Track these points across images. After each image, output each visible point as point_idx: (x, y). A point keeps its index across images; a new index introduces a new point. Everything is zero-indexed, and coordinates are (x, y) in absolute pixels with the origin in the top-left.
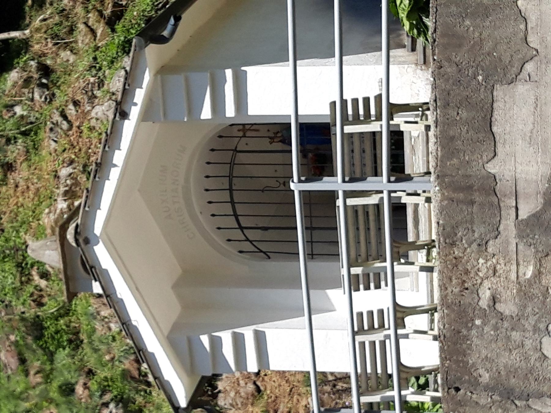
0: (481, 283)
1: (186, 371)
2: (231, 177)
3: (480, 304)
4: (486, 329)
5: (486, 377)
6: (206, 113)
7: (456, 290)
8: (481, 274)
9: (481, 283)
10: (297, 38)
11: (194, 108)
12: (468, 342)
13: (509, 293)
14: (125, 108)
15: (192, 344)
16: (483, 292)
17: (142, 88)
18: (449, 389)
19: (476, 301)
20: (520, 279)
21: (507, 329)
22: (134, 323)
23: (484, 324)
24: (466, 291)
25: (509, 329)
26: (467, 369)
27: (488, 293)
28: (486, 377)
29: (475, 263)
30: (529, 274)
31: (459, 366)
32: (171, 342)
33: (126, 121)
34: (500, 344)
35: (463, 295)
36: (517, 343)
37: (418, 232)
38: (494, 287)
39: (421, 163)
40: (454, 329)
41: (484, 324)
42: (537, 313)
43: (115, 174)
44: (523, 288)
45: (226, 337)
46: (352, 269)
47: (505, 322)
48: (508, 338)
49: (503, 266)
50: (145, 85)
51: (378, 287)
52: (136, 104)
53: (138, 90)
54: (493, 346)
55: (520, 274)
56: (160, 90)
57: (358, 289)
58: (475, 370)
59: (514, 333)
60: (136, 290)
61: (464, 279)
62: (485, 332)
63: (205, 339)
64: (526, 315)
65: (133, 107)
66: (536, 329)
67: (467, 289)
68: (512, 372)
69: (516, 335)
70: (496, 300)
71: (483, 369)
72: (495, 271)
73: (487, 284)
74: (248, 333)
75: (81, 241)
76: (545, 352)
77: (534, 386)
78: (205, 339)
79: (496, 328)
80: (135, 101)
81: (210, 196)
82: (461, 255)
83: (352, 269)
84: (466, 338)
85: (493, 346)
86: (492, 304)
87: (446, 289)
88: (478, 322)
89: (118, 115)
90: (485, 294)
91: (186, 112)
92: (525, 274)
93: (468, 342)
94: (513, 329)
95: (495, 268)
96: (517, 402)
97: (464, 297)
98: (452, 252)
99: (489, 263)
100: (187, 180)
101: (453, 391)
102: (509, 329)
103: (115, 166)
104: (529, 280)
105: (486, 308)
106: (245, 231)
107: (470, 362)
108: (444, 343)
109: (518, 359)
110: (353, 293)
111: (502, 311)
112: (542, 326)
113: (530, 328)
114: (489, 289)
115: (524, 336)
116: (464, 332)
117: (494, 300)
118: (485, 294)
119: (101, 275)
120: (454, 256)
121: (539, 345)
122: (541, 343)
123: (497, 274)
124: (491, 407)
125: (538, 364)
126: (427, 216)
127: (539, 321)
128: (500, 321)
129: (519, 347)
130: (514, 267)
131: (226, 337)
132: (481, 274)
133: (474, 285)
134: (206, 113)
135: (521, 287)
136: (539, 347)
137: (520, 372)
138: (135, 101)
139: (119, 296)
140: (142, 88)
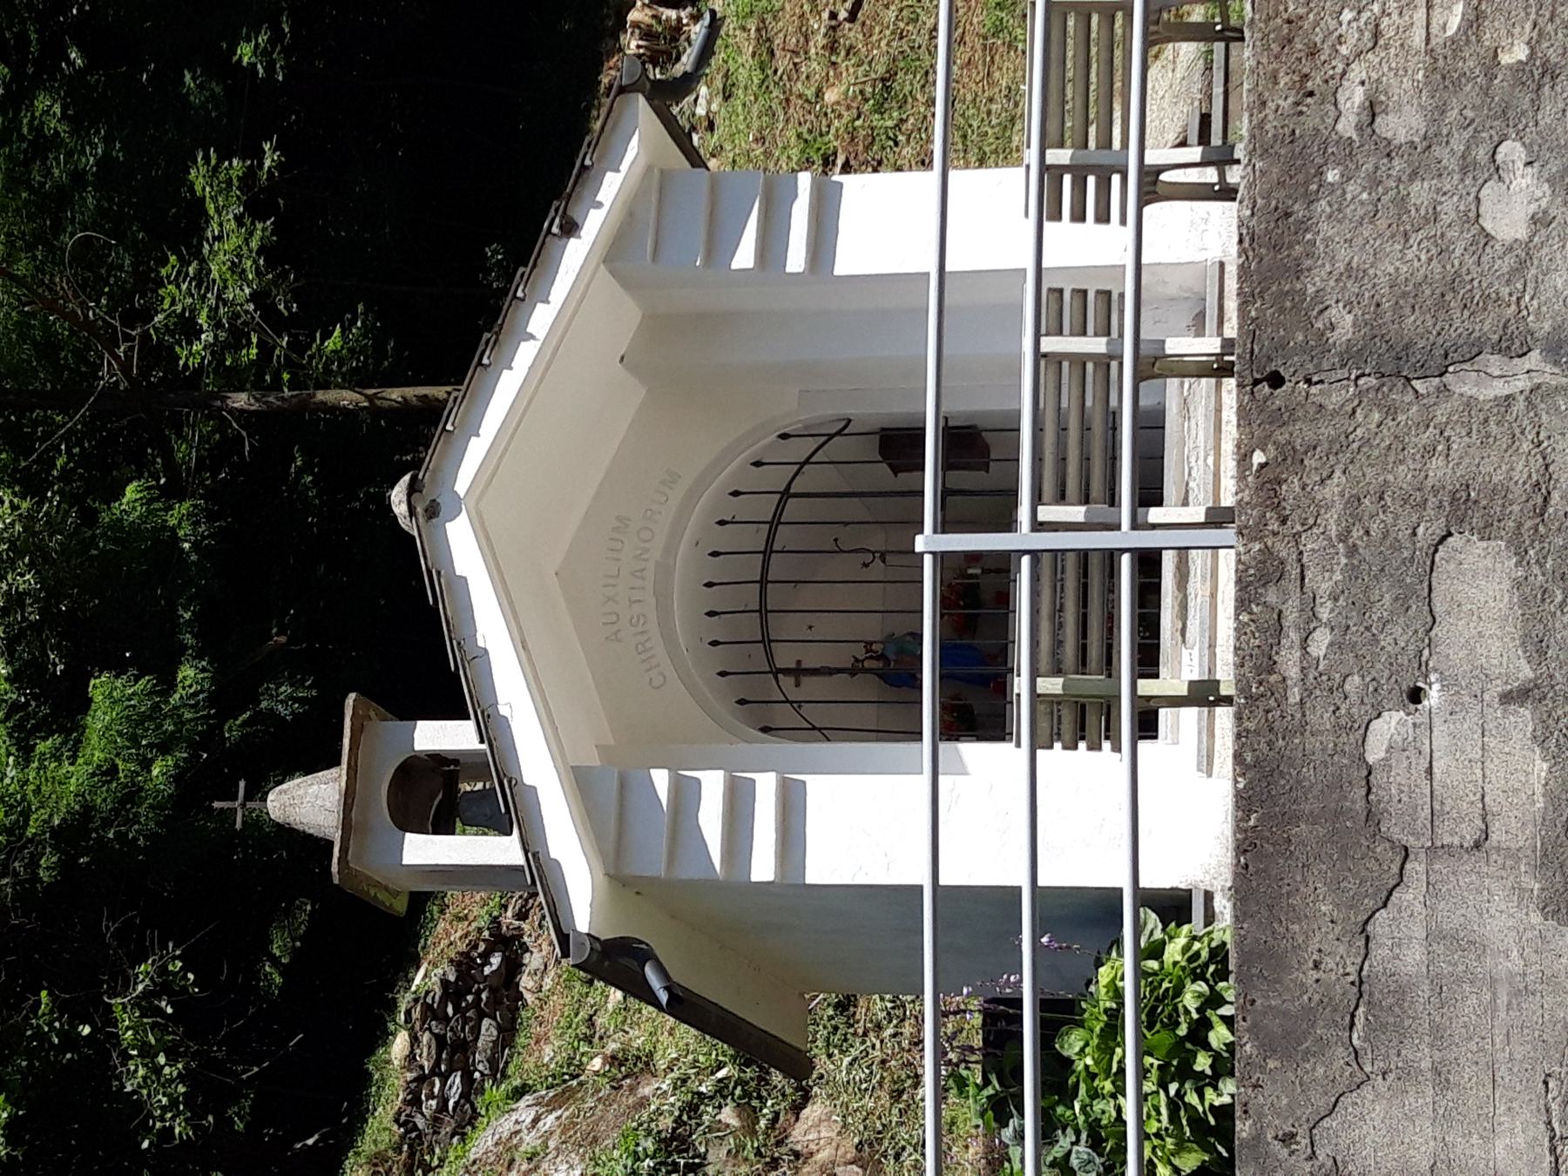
0: (1344, 73)
1: (602, 853)
2: (763, 611)
3: (1339, 127)
4: (1351, 188)
5: (1344, 324)
6: (744, 257)
7: (1286, 105)
8: (1344, 50)
9: (1344, 73)
10: (943, 384)
11: (719, 243)
12: (1308, 236)
13: (1407, 83)
14: (574, 213)
15: (629, 788)
16: (1347, 94)
17: (618, 171)
18: (1256, 382)
19: (1330, 121)
20: (1433, 42)
21: (1400, 179)
22: (503, 710)
23: (1347, 178)
24: (1309, 100)
25: (1404, 178)
26: (1303, 310)
27: (1359, 95)
28: (1344, 324)
29: (1333, 24)
30: (1454, 22)
31: (1282, 310)
32: (580, 782)
33: (573, 242)
34: (1382, 223)
35: (1301, 113)
36: (1423, 212)
37: (1185, 597)
38: (1374, 76)
39: (1201, 434)
40: (1276, 208)
41: (1347, 178)
42: (1473, 121)
43: (526, 354)
44: (1441, 62)
45: (712, 784)
46: (1039, 680)
47: (1396, 162)
48: (1402, 201)
49: (1395, 16)
50: (624, 167)
51: (1103, 217)
52: (599, 205)
53: (609, 176)
54: (1366, 234)
55: (1434, 30)
56: (654, 198)
57: (1057, 216)
58: (1321, 311)
59: (1416, 187)
60: (523, 646)
61: (1306, 70)
62: (1349, 197)
63: (661, 779)
64: (1445, 132)
65: (592, 211)
66: (1467, 166)
67: (1311, 94)
68: (1407, 294)
69: (1420, 193)
70: (1377, 110)
71: (1341, 305)
72: (1377, 35)
73: (1358, 72)
74: (766, 786)
75: (419, 510)
76: (1488, 226)
77: (1459, 324)
78: (661, 779)
79: (1374, 182)
80: (598, 198)
81: (715, 598)
82: (1301, 11)
83: (1039, 680)
84: (1304, 226)
85: (1366, 234)
86: (1366, 119)
87: (1264, 103)
88: (1332, 176)
89: (557, 221)
90: (1353, 97)
91: (702, 249)
92: (1444, 28)
93: (1308, 236)
94: (1413, 175)
95: (1377, 26)
96: (1417, 384)
97: (1303, 118)
98: (1282, 8)
99: (1365, 15)
100: (670, 550)
101: (1265, 388)
102: (1404, 178)
103: (532, 337)
104: (1453, 40)
105: (1354, 137)
106: (796, 467)
107: (1311, 290)
108: (1251, 254)
109: (1423, 257)
110: (1047, 225)
111: (1389, 135)
112: (1481, 154)
113: (1452, 163)
114: (1363, 83)
115: (1438, 191)
116: (1299, 209)
117: (1372, 109)
118: (1353, 97)
119: (467, 408)
120: (1285, 16)
121: (1473, 207)
122: (1478, 199)
123: (1381, 42)
124: (1354, 412)
125: (1470, 261)
126: (1210, 487)
127: (1475, 139)
128: (1385, 161)
129: (1427, 221)
130: (1421, 14)
131: (712, 784)
132: (1344, 50)
133: (1327, 81)
134: (744, 257)
135: (1436, 60)
136: (1472, 215)
137: (1428, 292)
138: (598, 198)
139: (481, 643)
140: (618, 171)
